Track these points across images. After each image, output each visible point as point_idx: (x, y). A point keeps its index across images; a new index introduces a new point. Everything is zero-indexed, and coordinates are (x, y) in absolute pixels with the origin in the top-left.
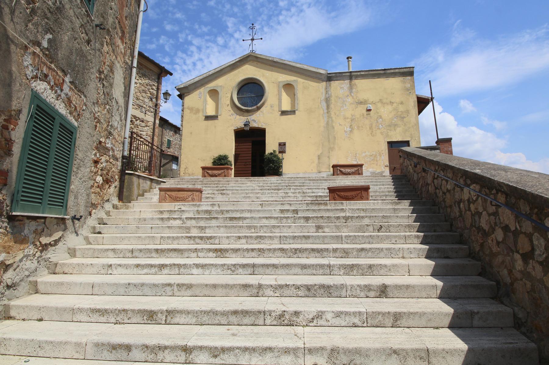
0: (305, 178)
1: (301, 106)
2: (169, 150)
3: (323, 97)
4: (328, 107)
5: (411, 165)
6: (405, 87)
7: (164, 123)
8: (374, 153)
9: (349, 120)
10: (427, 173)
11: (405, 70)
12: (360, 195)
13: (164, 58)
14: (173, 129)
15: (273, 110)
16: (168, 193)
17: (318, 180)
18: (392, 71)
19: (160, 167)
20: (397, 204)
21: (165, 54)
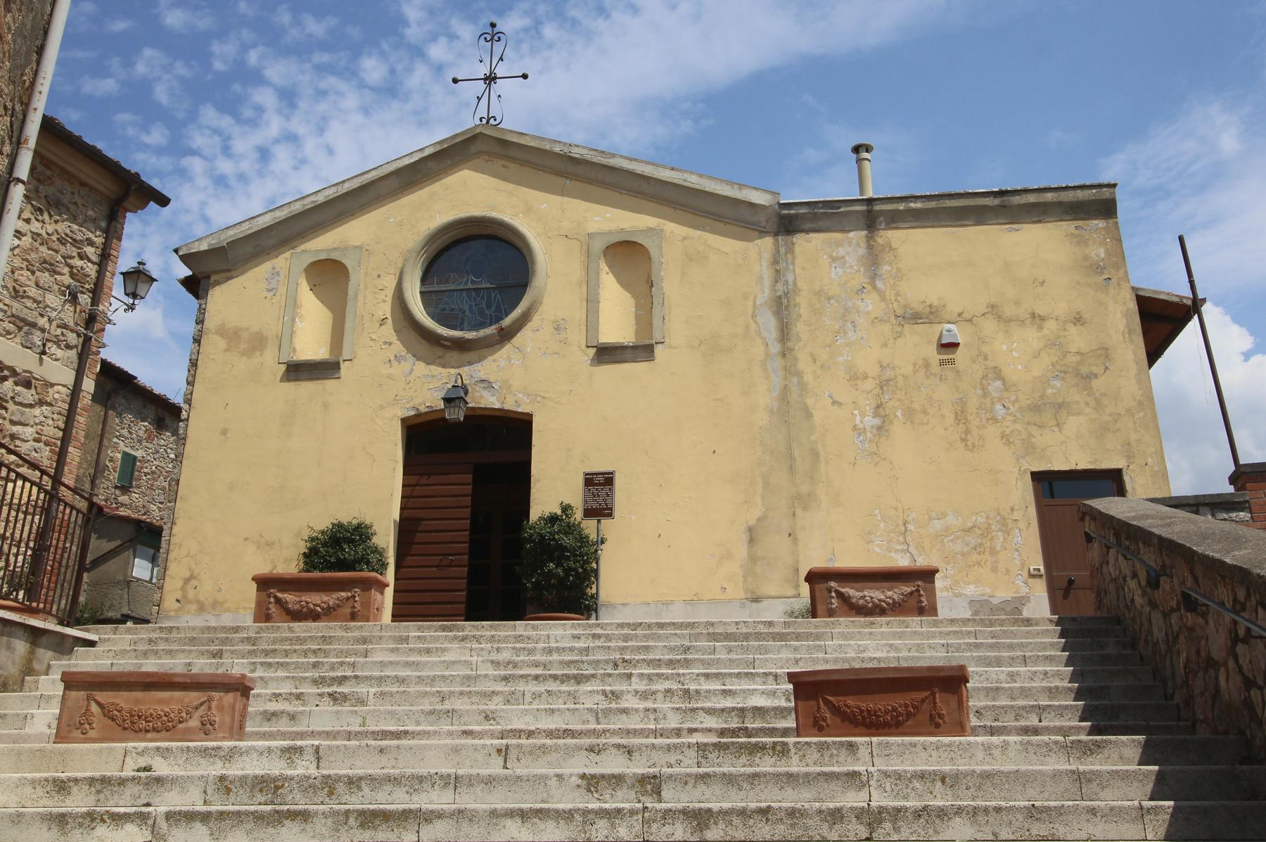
0: (691, 625)
1: (676, 326)
2: (124, 499)
3: (764, 295)
4: (785, 333)
5: (1135, 575)
6: (1086, 258)
7: (118, 386)
8: (981, 520)
9: (869, 384)
10: (1204, 615)
11: (1081, 195)
12: (926, 707)
13: (145, 128)
14: (151, 411)
15: (564, 342)
16: (102, 696)
17: (746, 637)
18: (1032, 198)
19: (82, 568)
20: (1088, 750)
21: (150, 112)
